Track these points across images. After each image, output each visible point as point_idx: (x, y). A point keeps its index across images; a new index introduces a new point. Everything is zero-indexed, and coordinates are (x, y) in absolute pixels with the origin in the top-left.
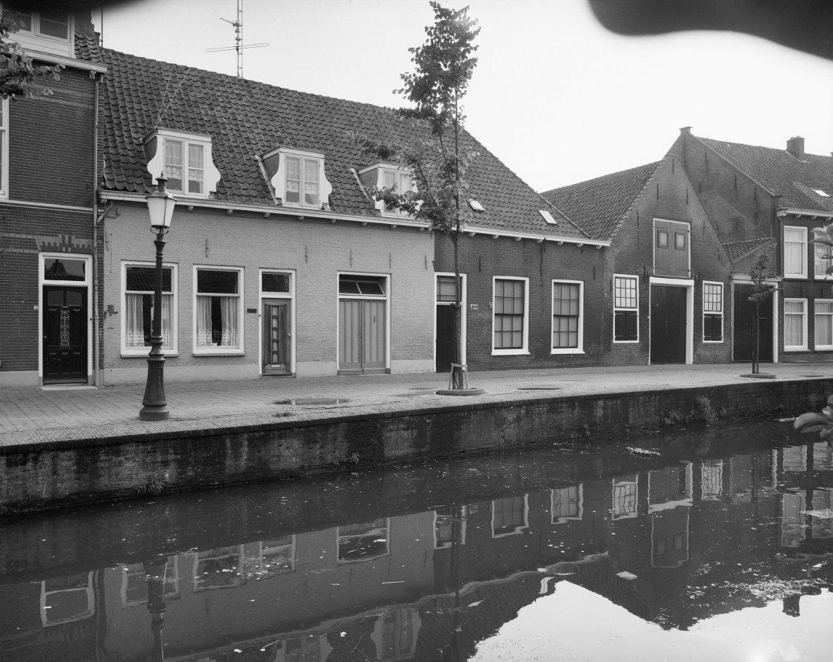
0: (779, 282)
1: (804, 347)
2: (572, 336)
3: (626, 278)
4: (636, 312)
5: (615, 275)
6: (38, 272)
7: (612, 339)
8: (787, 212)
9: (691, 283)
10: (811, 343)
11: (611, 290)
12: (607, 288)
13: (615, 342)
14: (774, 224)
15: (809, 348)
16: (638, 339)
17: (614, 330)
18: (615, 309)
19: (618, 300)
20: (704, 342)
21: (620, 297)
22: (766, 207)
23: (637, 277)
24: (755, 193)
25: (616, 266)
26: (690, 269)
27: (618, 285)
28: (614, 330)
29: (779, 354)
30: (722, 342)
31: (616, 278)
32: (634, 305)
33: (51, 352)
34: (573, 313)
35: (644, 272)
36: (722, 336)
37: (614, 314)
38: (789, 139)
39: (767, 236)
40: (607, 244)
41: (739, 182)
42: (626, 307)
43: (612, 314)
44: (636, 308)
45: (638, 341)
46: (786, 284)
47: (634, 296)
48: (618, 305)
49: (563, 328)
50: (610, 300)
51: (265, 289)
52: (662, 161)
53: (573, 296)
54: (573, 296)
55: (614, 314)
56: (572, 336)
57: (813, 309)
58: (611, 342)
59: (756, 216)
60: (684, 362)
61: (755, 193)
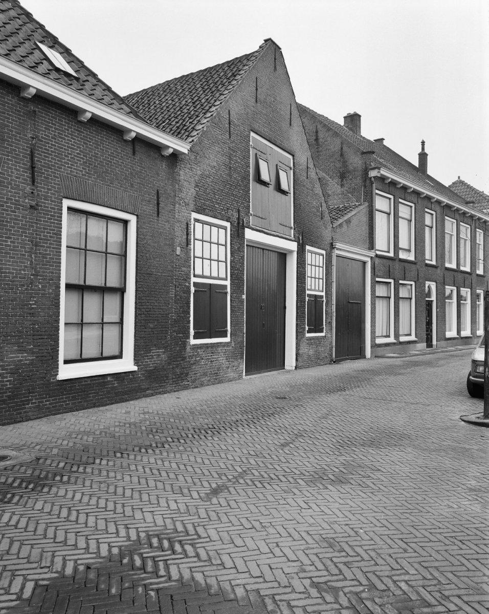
0: (372, 258)
1: (392, 339)
2: (111, 333)
3: (211, 225)
4: (225, 287)
5: (194, 215)
6: (135, 342)
7: (188, 337)
8: (382, 172)
9: (293, 246)
10: (459, 332)
11: (188, 242)
12: (180, 238)
13: (193, 342)
14: (365, 187)
15: (471, 334)
16: (229, 335)
17: (192, 319)
18: (194, 280)
19: (198, 262)
20: (308, 335)
21: (203, 258)
22: (355, 165)
23: (228, 225)
24: (342, 149)
25: (197, 197)
26: (292, 225)
27: (198, 235)
28: (192, 319)
29: (372, 347)
30: (227, 340)
31: (197, 220)
32: (223, 275)
33: (313, 329)
34: (113, 282)
35: (238, 219)
36: (324, 326)
37: (193, 289)
38: (346, 115)
39: (357, 201)
40: (182, 147)
41: (321, 135)
42: (211, 278)
43: (189, 288)
44: (226, 279)
45: (227, 340)
46: (377, 261)
47: (222, 258)
48: (198, 271)
49: (91, 314)
50: (186, 261)
51: (278, 362)
52: (257, 52)
53: (111, 316)
54: (111, 316)
55: (193, 289)
56: (111, 333)
57: (398, 293)
58: (185, 344)
59: (342, 177)
60: (282, 365)
61: (342, 149)
